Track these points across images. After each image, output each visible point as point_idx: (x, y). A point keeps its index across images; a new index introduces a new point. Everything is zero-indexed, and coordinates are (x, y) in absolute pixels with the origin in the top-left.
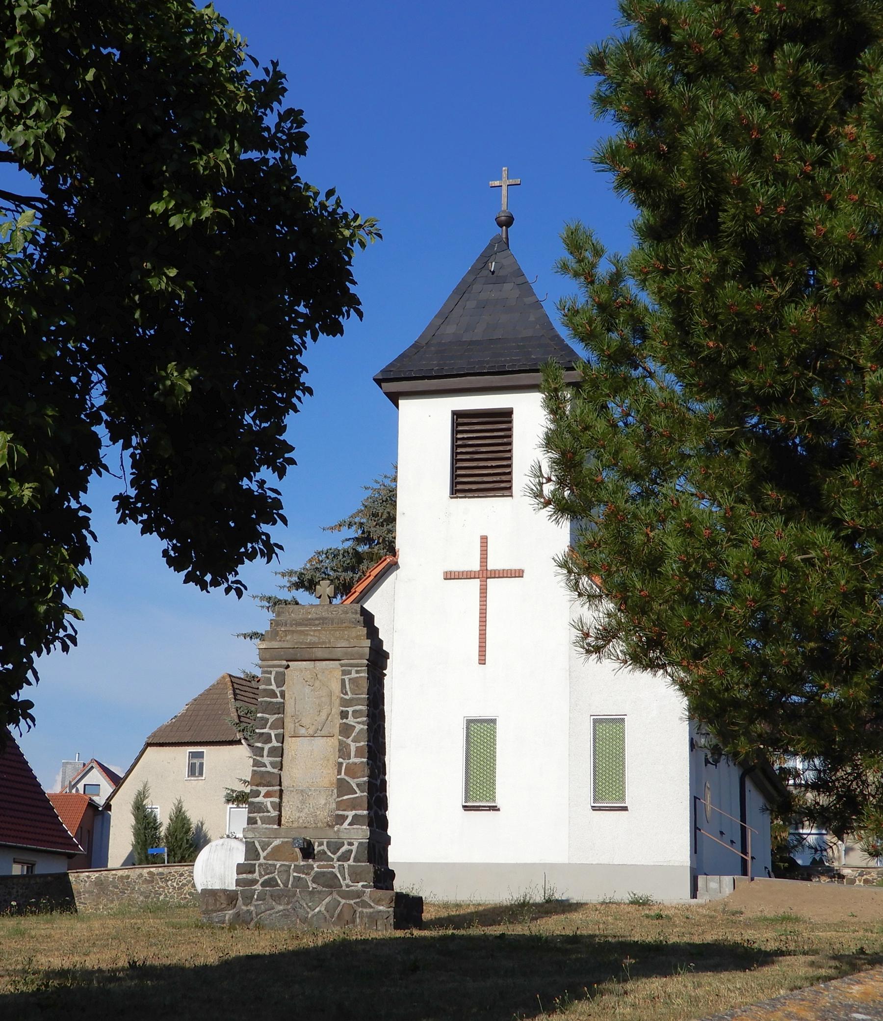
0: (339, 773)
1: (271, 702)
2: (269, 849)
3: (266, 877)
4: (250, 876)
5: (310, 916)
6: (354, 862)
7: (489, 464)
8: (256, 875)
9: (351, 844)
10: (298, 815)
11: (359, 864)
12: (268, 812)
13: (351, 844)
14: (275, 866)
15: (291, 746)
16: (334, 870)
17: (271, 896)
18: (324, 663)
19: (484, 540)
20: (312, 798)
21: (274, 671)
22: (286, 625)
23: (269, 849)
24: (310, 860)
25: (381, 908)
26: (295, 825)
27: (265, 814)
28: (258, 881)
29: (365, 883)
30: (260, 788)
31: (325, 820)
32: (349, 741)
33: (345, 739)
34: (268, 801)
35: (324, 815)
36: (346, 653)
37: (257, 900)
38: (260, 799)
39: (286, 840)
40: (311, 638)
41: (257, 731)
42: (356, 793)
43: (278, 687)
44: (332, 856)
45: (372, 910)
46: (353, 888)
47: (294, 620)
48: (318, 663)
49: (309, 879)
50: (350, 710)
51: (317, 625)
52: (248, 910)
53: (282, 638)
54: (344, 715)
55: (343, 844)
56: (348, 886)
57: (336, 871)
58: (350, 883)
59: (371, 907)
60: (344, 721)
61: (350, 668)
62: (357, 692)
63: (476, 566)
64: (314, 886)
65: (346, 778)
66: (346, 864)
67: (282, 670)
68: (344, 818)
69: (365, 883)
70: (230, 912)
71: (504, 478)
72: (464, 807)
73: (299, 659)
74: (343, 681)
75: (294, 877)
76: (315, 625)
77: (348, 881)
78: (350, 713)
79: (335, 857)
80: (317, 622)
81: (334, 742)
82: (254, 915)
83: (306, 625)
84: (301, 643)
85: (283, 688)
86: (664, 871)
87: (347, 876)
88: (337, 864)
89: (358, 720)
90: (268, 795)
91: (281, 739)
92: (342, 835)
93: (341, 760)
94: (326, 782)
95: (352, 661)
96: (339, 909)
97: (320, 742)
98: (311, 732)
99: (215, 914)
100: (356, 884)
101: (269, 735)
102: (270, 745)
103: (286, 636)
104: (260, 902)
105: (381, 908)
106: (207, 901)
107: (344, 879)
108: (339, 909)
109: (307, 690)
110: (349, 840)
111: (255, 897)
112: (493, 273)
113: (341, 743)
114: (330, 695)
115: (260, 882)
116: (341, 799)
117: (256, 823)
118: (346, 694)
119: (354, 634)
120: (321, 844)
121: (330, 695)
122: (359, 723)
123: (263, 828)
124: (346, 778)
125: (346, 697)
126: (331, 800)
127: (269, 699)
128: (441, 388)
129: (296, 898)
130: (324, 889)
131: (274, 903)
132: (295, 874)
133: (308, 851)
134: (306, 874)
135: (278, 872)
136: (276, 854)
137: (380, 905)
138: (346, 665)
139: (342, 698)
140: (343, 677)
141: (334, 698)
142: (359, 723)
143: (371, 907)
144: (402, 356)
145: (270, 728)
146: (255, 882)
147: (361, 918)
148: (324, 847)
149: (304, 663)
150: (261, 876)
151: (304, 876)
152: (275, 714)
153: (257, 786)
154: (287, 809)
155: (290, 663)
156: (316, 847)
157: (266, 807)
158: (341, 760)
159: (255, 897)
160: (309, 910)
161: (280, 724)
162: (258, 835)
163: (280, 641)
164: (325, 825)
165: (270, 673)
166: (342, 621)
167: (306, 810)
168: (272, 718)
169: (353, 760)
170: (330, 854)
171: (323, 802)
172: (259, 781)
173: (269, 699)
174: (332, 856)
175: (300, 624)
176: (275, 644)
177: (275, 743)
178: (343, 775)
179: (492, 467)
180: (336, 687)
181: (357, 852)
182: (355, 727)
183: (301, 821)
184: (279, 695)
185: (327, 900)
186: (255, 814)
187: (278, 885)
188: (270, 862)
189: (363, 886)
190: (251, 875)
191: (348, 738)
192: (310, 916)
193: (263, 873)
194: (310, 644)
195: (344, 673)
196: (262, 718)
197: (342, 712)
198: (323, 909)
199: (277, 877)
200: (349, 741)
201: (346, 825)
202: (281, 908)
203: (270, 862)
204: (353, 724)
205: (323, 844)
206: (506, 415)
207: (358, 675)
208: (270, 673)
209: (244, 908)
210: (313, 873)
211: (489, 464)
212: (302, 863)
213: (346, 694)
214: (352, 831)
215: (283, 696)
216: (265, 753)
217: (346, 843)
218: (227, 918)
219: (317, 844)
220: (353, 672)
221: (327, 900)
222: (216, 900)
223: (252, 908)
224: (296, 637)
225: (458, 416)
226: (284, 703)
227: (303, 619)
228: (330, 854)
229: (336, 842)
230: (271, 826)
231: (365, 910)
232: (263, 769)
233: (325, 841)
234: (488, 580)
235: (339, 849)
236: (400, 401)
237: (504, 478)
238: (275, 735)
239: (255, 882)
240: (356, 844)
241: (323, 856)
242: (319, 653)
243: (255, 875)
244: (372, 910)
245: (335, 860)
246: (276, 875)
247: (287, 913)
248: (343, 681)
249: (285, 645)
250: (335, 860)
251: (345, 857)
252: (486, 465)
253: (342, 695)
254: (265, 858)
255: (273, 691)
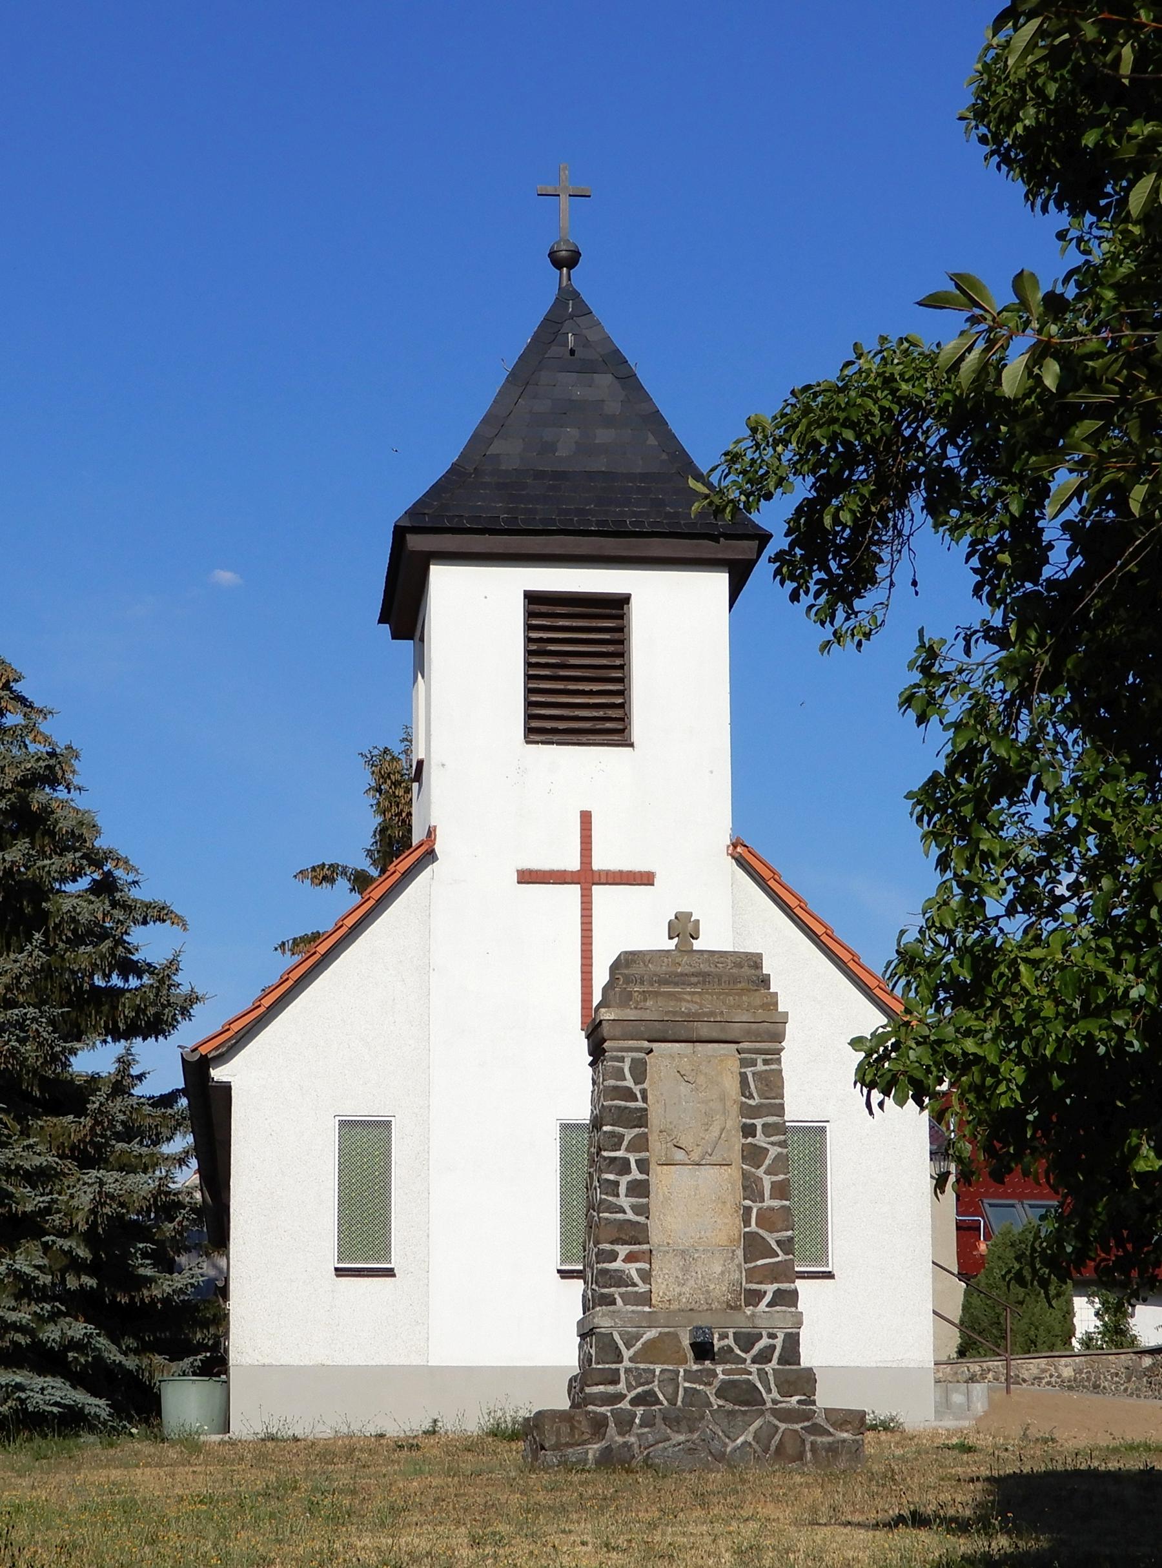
0: (747, 1223)
1: (626, 1108)
2: (639, 1344)
3: (640, 1390)
4: (611, 1389)
5: (729, 1449)
6: (778, 1364)
7: (587, 687)
8: (621, 1387)
9: (772, 1336)
10: (678, 1290)
11: (788, 1367)
12: (635, 1285)
13: (772, 1336)
14: (654, 1371)
15: (662, 1179)
16: (750, 1377)
17: (664, 1419)
18: (710, 1045)
19: (586, 818)
20: (699, 1263)
21: (629, 1057)
22: (642, 983)
23: (639, 1344)
24: (707, 1362)
25: (845, 1435)
26: (675, 1306)
27: (629, 1289)
28: (625, 1396)
29: (803, 1398)
30: (617, 1248)
31: (724, 1299)
32: (760, 1172)
33: (753, 1170)
34: (632, 1269)
35: (720, 1291)
36: (748, 1032)
37: (641, 1426)
38: (617, 1265)
39: (667, 1330)
40: (690, 1006)
41: (605, 1154)
42: (778, 1256)
43: (636, 1083)
44: (743, 1355)
45: (830, 1439)
46: (783, 1405)
47: (655, 975)
48: (700, 1047)
49: (710, 1391)
50: (759, 1123)
51: (695, 985)
52: (625, 1443)
53: (637, 1003)
54: (748, 1131)
55: (760, 1336)
56: (775, 1402)
57: (754, 1378)
58: (779, 1398)
59: (831, 1434)
60: (750, 1140)
61: (754, 1056)
62: (768, 1095)
63: (573, 863)
64: (721, 1402)
65: (761, 1231)
66: (768, 1368)
67: (642, 1055)
68: (760, 1295)
69: (803, 1398)
70: (595, 1446)
71: (611, 713)
72: (337, 1269)
73: (671, 1038)
74: (743, 1077)
75: (685, 1389)
76: (690, 984)
77: (775, 1395)
78: (759, 1128)
79: (748, 1357)
80: (694, 980)
81: (733, 1174)
82: (636, 1450)
83: (676, 984)
84: (674, 1013)
85: (645, 1086)
86: (539, 1374)
87: (773, 1386)
88: (754, 1368)
89: (772, 1139)
90: (630, 1258)
91: (643, 1166)
92: (759, 1322)
93: (748, 1203)
94: (722, 1239)
95: (758, 1045)
96: (777, 1437)
97: (709, 1174)
98: (695, 1157)
99: (571, 1450)
100: (788, 1399)
101: (626, 1162)
102: (629, 1178)
103: (645, 1000)
104: (646, 1430)
105: (845, 1435)
106: (558, 1429)
107: (769, 1391)
108: (777, 1437)
109: (684, 1089)
110: (770, 1330)
111: (637, 1421)
112: (572, 352)
113: (745, 1175)
114: (723, 1098)
115: (628, 1398)
116: (752, 1265)
117: (613, 1303)
118: (751, 1097)
119: (758, 1002)
120: (724, 1336)
121: (723, 1098)
122: (772, 1144)
123: (627, 1312)
124: (761, 1231)
125: (751, 1102)
126: (732, 1266)
127: (623, 1103)
128: (511, 551)
129: (705, 1423)
130: (737, 1407)
131: (669, 1431)
132: (687, 1385)
133: (703, 1350)
134: (706, 1384)
135: (659, 1381)
136: (651, 1352)
137: (842, 1430)
138: (749, 1051)
139: (743, 1103)
140: (743, 1070)
141: (729, 1103)
142: (772, 1144)
143: (831, 1434)
144: (437, 490)
145: (627, 1150)
146: (620, 1397)
147: (814, 1450)
148: (730, 1341)
149: (677, 1045)
150: (630, 1387)
151: (702, 1387)
152: (635, 1127)
153: (612, 1243)
154: (660, 1281)
155: (654, 1045)
156: (715, 1341)
157: (630, 1277)
158: (748, 1203)
159: (637, 1421)
160: (727, 1440)
161: (640, 1143)
162: (620, 1323)
163: (636, 1008)
164: (725, 1306)
165: (622, 1060)
166: (735, 980)
167: (692, 1283)
168: (629, 1134)
169: (769, 1203)
170: (739, 1352)
171: (718, 1269)
172: (615, 1235)
173: (623, 1103)
174: (743, 1355)
175: (663, 982)
176: (630, 1014)
177: (636, 1174)
178: (753, 1227)
179: (591, 693)
180: (731, 1085)
181: (783, 1348)
182: (768, 1150)
183: (684, 1300)
184: (639, 1096)
185: (757, 1424)
186: (612, 1289)
187: (658, 1402)
188: (642, 1366)
189: (799, 1402)
190: (612, 1387)
191: (759, 1167)
192: (729, 1449)
193: (634, 1383)
194: (688, 1015)
195: (744, 1063)
196: (612, 1134)
197: (745, 1125)
198: (750, 1439)
199: (656, 1389)
200: (760, 1172)
201: (763, 1306)
202: (682, 1438)
203: (642, 1366)
204: (765, 1145)
205: (727, 1337)
206: (618, 605)
207: (767, 1067)
208: (622, 1060)
209: (620, 1440)
210: (716, 1383)
211: (587, 687)
212: (695, 1367)
213: (751, 1097)
214: (777, 1315)
215: (645, 1099)
216: (622, 1189)
217: (764, 1333)
218: (590, 1456)
219: (716, 1336)
220: (759, 1062)
221: (757, 1424)
222: (573, 1428)
223: (633, 1439)
224: (661, 1002)
225: (531, 598)
226: (646, 1110)
227: (671, 974)
228: (739, 1352)
229: (749, 1334)
230: (639, 1308)
231: (819, 1439)
232: (620, 1216)
233: (731, 1332)
234: (594, 887)
235: (753, 1345)
236: (432, 567)
237: (611, 713)
238: (636, 1161)
239: (620, 1397)
240: (781, 1336)
241: (728, 1356)
242: (705, 1031)
243: (618, 1386)
244: (830, 1439)
245: (749, 1361)
246: (655, 1386)
247: (693, 1446)
248: (743, 1077)
249: (647, 1015)
250: (749, 1361)
251: (764, 1357)
252: (581, 688)
253: (744, 1099)
254: (631, 1360)
255: (629, 1089)
